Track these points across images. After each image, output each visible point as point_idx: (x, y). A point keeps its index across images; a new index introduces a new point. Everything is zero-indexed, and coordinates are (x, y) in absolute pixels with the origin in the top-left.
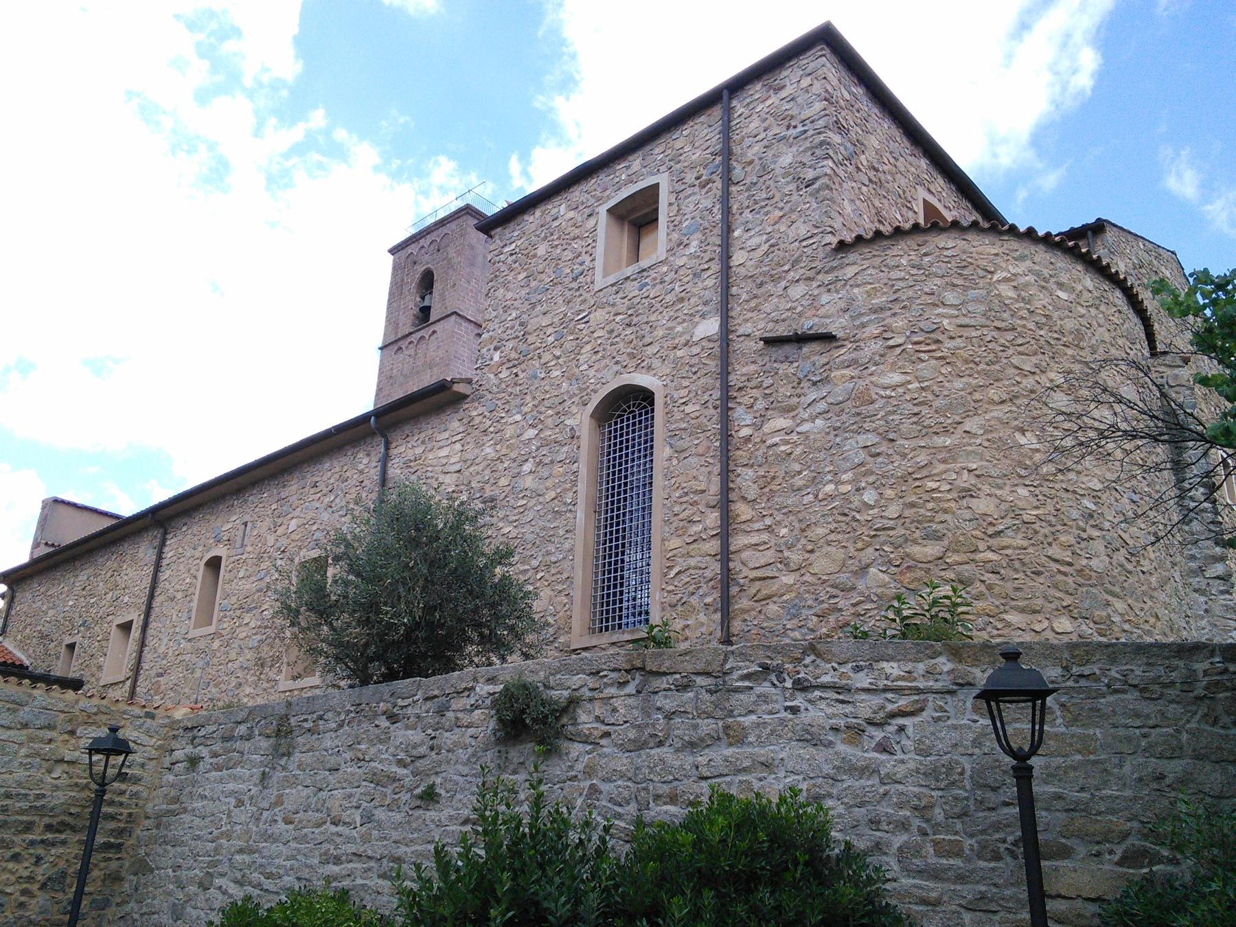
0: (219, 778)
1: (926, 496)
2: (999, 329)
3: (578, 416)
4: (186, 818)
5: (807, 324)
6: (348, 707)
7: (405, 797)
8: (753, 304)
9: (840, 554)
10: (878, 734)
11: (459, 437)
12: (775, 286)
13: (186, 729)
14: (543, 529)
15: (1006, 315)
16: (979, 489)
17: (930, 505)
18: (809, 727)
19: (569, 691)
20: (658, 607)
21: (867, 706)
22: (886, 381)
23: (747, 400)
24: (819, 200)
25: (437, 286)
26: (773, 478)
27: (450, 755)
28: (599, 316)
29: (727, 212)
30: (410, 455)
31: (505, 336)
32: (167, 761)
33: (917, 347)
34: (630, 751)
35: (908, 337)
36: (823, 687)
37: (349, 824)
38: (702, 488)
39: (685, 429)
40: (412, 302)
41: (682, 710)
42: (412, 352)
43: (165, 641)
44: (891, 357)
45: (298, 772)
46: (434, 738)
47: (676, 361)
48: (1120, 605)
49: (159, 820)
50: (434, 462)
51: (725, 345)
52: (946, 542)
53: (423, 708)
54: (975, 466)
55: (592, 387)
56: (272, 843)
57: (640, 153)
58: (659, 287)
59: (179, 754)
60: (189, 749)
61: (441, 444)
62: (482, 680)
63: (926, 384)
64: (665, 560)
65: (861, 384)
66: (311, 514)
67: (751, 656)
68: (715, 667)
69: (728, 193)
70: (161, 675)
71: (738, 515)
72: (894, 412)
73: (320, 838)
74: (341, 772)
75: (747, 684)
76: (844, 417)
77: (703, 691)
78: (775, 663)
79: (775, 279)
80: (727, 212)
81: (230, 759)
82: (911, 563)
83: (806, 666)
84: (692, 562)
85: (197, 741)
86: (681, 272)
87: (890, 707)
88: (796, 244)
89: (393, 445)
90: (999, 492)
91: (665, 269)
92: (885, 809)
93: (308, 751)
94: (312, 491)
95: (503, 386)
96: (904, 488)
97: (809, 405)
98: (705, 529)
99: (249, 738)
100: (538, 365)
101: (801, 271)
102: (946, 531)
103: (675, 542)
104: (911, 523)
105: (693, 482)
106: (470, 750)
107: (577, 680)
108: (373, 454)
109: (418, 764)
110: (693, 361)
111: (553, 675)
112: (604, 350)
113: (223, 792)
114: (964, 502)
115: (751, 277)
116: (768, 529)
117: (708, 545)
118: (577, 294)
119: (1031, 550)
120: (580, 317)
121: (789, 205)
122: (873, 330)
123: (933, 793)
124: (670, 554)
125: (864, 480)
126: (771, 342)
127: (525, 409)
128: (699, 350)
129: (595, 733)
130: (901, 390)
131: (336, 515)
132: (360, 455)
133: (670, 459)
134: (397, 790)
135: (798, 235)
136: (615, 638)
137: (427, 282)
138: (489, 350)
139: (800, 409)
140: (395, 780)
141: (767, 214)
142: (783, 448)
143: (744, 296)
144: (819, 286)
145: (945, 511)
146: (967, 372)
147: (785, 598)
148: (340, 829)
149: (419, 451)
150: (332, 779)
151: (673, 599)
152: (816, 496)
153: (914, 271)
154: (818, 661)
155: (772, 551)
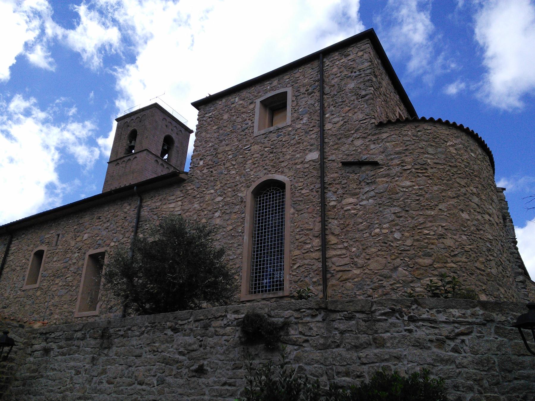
0: (64, 360)
1: (424, 237)
2: (450, 166)
3: (245, 192)
4: (43, 380)
5: (364, 157)
6: (147, 324)
7: (185, 371)
8: (336, 147)
9: (384, 261)
10: (452, 344)
11: (180, 199)
12: (347, 140)
13: (41, 334)
14: (226, 243)
15: (453, 161)
16: (446, 235)
17: (426, 241)
18: (418, 340)
19: (283, 319)
20: (288, 282)
21: (446, 330)
22: (403, 184)
23: (333, 189)
24: (369, 104)
25: (138, 138)
26: (348, 225)
27: (212, 350)
28: (256, 148)
29: (322, 107)
30: (153, 205)
31: (205, 154)
32: (29, 350)
33: (417, 171)
34: (321, 350)
35: (413, 166)
36: (423, 320)
37: (150, 384)
38: (311, 228)
39: (301, 201)
40: (125, 142)
41: (350, 329)
42: (124, 165)
43: (8, 291)
44: (405, 174)
45: (116, 357)
46: (202, 341)
47: (296, 170)
48: (502, 290)
49: (25, 381)
50: (167, 210)
51: (322, 164)
52: (433, 258)
53: (194, 325)
54: (444, 225)
55: (252, 179)
56: (100, 394)
57: (277, 78)
58: (287, 136)
59: (37, 347)
60: (44, 344)
61: (171, 201)
62: (230, 312)
63: (421, 187)
64: (291, 260)
65: (392, 185)
66: (96, 232)
67: (385, 304)
68: (367, 309)
69: (323, 98)
70: (5, 308)
71: (329, 241)
72: (408, 199)
73: (132, 392)
74: (143, 357)
75: (384, 317)
76: (383, 199)
77: (361, 321)
78: (398, 308)
79: (347, 137)
80: (322, 107)
81: (71, 350)
82: (418, 266)
83: (413, 310)
84: (306, 262)
85: (49, 340)
86: (299, 131)
87: (457, 331)
88: (357, 122)
89: (144, 201)
90: (455, 237)
91: (290, 129)
92: (460, 380)
93: (122, 346)
94: (98, 220)
95: (205, 176)
96: (413, 232)
97: (366, 193)
98: (313, 247)
99: (83, 339)
100: (223, 168)
101: (360, 134)
102: (433, 253)
103: (297, 252)
104: (417, 248)
105: (306, 225)
106: (225, 348)
107: (287, 313)
108: (132, 205)
109: (193, 354)
110: (305, 171)
111: (274, 310)
112: (259, 163)
113: (67, 367)
114: (440, 241)
115: (335, 135)
116: (346, 248)
117: (314, 254)
118: (244, 137)
119: (469, 263)
120: (246, 148)
121: (353, 105)
122: (397, 162)
123: (482, 373)
124: (294, 258)
125: (394, 228)
126: (345, 164)
127: (216, 188)
128: (308, 166)
129: (300, 340)
130: (410, 189)
131: (111, 233)
132: (126, 205)
133: (293, 214)
134: (180, 367)
135: (358, 118)
136: (265, 296)
137: (133, 135)
138: (197, 160)
139: (361, 195)
140: (177, 362)
141: (342, 108)
142: (353, 212)
143: (331, 143)
144: (369, 141)
145: (433, 244)
146: (439, 183)
147: (356, 280)
148: (144, 387)
149: (158, 204)
150: (138, 361)
151: (296, 279)
152: (370, 234)
153: (414, 138)
154: (419, 307)
155: (348, 259)
